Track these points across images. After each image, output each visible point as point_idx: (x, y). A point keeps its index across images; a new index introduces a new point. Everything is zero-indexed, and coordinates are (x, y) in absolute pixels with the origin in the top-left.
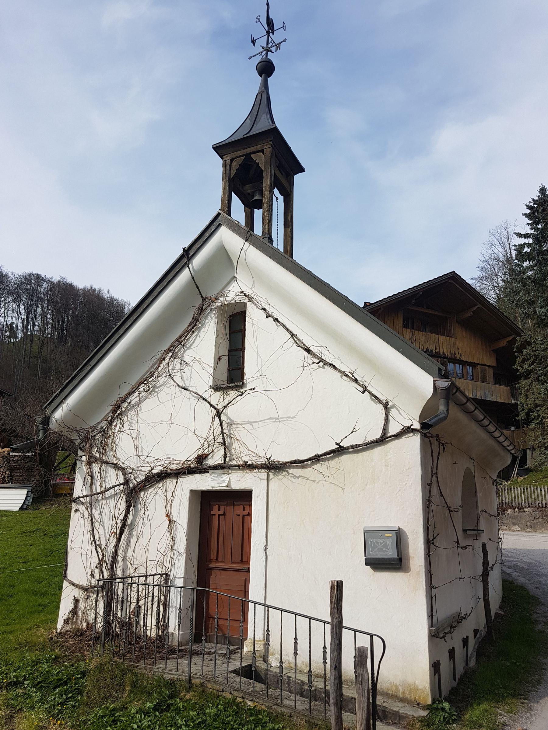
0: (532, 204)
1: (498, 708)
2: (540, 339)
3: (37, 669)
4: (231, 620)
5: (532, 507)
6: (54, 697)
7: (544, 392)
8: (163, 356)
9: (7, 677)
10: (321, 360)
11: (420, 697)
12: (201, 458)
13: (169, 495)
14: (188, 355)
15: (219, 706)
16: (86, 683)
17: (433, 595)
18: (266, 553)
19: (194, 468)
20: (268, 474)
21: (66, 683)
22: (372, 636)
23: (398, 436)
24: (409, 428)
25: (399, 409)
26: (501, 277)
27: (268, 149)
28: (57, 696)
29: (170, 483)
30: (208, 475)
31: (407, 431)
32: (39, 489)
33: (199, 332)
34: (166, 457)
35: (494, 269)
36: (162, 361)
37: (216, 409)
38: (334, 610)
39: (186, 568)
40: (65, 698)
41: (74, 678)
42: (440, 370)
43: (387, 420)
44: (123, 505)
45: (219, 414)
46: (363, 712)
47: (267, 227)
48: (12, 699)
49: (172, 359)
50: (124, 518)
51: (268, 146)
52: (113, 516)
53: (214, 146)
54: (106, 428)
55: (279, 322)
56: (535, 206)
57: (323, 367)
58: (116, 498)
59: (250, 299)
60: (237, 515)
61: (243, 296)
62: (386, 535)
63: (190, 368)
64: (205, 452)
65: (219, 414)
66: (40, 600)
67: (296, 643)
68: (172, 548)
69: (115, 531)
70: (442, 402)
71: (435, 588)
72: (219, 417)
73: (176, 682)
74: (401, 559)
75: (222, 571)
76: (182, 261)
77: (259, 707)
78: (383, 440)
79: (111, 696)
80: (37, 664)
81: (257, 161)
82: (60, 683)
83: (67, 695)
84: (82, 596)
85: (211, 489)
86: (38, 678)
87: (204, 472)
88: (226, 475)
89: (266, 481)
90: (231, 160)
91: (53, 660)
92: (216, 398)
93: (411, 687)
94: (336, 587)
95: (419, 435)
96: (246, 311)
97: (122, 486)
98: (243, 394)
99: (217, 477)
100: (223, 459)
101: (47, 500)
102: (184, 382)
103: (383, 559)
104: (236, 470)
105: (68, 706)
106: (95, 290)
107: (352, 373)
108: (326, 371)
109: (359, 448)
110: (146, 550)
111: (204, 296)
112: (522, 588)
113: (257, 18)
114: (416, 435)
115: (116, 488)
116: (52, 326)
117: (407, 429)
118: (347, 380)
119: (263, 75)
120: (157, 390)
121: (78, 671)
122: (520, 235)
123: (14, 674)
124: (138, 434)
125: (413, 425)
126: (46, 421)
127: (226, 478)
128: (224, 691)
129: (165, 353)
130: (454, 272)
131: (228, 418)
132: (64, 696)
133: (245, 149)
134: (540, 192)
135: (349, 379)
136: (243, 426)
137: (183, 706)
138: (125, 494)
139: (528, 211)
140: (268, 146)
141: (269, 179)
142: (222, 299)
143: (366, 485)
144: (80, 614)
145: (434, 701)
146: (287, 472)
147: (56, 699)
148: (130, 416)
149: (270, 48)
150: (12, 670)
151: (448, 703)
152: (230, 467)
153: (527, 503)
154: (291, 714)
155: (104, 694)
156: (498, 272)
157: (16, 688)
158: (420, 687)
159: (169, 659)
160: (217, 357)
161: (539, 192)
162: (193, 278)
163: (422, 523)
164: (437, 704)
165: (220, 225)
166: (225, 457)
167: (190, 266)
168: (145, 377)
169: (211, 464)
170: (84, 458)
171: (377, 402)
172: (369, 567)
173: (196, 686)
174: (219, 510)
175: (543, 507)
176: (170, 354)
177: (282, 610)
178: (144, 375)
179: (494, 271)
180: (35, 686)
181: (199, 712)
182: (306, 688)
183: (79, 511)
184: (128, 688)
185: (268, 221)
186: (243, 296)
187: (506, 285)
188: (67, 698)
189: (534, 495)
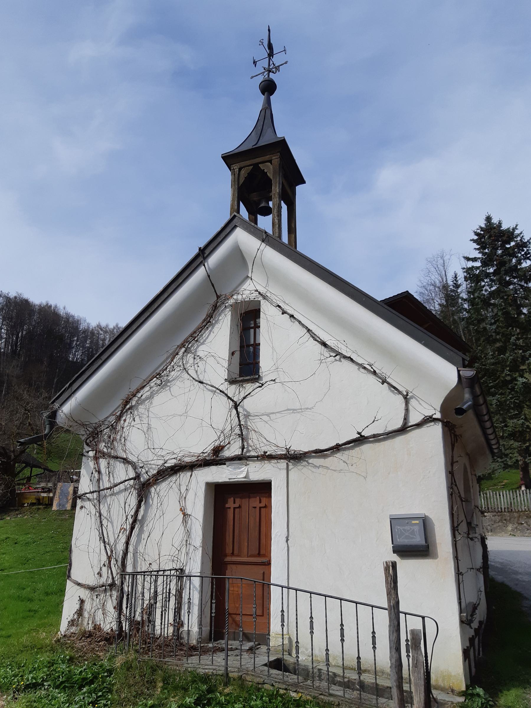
0: (479, 231)
1: (527, 694)
2: (490, 354)
3: (55, 670)
4: (243, 615)
5: (492, 512)
6: (83, 696)
7: (496, 402)
8: (176, 351)
9: (22, 679)
10: (338, 354)
11: (453, 683)
12: (217, 450)
13: (183, 489)
14: (202, 350)
15: (264, 698)
16: (113, 682)
17: (460, 581)
18: (288, 544)
19: (210, 460)
20: (287, 463)
21: (92, 682)
22: (423, 618)
23: (419, 425)
24: (431, 417)
25: (419, 399)
26: (438, 301)
27: (276, 159)
28: (86, 695)
29: (184, 477)
30: (225, 466)
31: (428, 420)
32: (4, 499)
33: (213, 328)
34: (179, 450)
35: (431, 294)
36: (175, 355)
37: (233, 401)
38: (390, 591)
39: (203, 563)
40: (95, 697)
41: (100, 676)
42: (464, 360)
43: (407, 410)
44: (133, 501)
45: (236, 406)
46: (421, 694)
47: (277, 230)
48: (35, 702)
49: (185, 354)
50: (135, 513)
51: (277, 157)
52: (124, 511)
53: (223, 156)
54: (114, 423)
55: (295, 318)
56: (482, 232)
57: (340, 360)
58: (127, 493)
59: (265, 297)
60: (254, 507)
61: (257, 295)
62: (413, 522)
63: (204, 362)
64: (221, 444)
65: (236, 406)
66: (30, 605)
67: (342, 630)
68: (187, 543)
69: (125, 527)
70: (467, 390)
71: (463, 575)
72: (236, 408)
73: (211, 677)
74: (428, 546)
75: (237, 566)
76: (197, 261)
77: (304, 698)
78: (404, 429)
79: (143, 693)
80: (53, 665)
81: (265, 171)
82: (84, 682)
83: (96, 694)
84: (89, 596)
85: (228, 480)
86: (59, 678)
87: (221, 464)
88: (243, 466)
89: (285, 471)
90: (239, 169)
91: (69, 660)
92: (232, 390)
93: (445, 674)
94: (391, 568)
95: (440, 424)
96: (260, 309)
97: (132, 481)
98: (263, 385)
99: (234, 469)
100: (240, 450)
101: (12, 510)
102: (198, 376)
103: (411, 546)
104: (254, 461)
105: (99, 705)
106: (51, 306)
107: (370, 366)
108: (343, 364)
109: (379, 438)
110: (159, 545)
111: (219, 294)
112: (502, 584)
114: (437, 424)
115: (126, 483)
116: (6, 341)
117: (428, 419)
118: (364, 372)
119: (266, 94)
120: (169, 384)
121: (103, 670)
122: (468, 259)
123: (31, 675)
124: (149, 428)
125: (435, 414)
126: (54, 415)
127: (244, 469)
128: (265, 683)
129: (178, 348)
130: (407, 291)
131: (245, 410)
132: (93, 695)
133: (253, 159)
134: (486, 220)
135: (366, 372)
136: (260, 417)
137: (225, 699)
138: (135, 488)
139: (476, 237)
140: (277, 157)
141: (278, 187)
142: (235, 297)
143: (389, 473)
144: (86, 615)
145: (467, 687)
146: (307, 462)
147: (86, 698)
148: (140, 410)
150: (27, 672)
151: (481, 689)
152: (248, 458)
153: (487, 507)
154: (339, 702)
155: (135, 691)
156: (435, 297)
157: (35, 690)
158: (453, 674)
159: (192, 656)
160: (231, 353)
161: (486, 220)
162: (209, 276)
163: (448, 510)
164: (471, 690)
165: (235, 227)
166: (243, 449)
167: (206, 264)
168: (158, 371)
169: (227, 456)
170: (91, 454)
171: (396, 393)
172: (395, 554)
173: (234, 680)
174: (234, 503)
175: (502, 512)
176: (183, 349)
177: (326, 596)
178: (155, 370)
179: (431, 295)
180: (57, 687)
181: (244, 704)
182: (338, 680)
183: (85, 507)
184: (160, 684)
185: (277, 226)
186: (257, 295)
187: (442, 308)
188: (98, 697)
189: (494, 500)
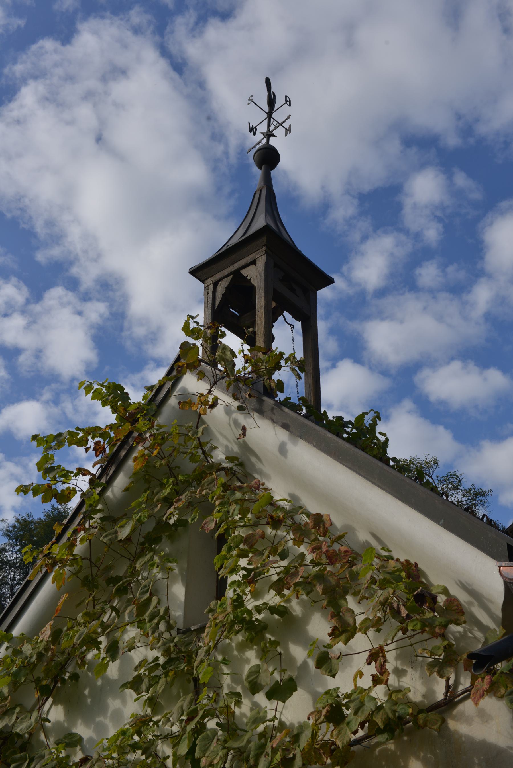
113: (249, 100)
149: (272, 132)
